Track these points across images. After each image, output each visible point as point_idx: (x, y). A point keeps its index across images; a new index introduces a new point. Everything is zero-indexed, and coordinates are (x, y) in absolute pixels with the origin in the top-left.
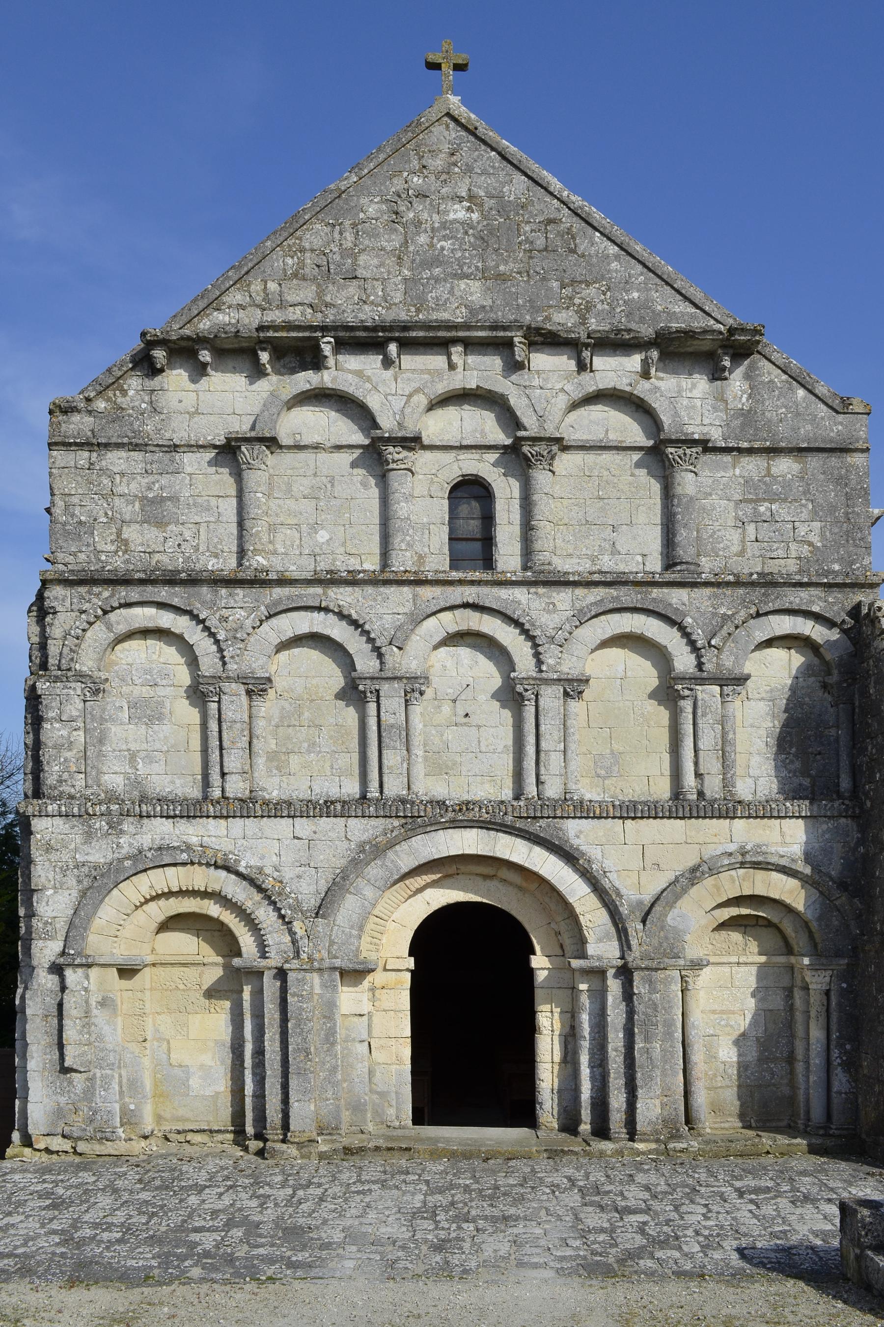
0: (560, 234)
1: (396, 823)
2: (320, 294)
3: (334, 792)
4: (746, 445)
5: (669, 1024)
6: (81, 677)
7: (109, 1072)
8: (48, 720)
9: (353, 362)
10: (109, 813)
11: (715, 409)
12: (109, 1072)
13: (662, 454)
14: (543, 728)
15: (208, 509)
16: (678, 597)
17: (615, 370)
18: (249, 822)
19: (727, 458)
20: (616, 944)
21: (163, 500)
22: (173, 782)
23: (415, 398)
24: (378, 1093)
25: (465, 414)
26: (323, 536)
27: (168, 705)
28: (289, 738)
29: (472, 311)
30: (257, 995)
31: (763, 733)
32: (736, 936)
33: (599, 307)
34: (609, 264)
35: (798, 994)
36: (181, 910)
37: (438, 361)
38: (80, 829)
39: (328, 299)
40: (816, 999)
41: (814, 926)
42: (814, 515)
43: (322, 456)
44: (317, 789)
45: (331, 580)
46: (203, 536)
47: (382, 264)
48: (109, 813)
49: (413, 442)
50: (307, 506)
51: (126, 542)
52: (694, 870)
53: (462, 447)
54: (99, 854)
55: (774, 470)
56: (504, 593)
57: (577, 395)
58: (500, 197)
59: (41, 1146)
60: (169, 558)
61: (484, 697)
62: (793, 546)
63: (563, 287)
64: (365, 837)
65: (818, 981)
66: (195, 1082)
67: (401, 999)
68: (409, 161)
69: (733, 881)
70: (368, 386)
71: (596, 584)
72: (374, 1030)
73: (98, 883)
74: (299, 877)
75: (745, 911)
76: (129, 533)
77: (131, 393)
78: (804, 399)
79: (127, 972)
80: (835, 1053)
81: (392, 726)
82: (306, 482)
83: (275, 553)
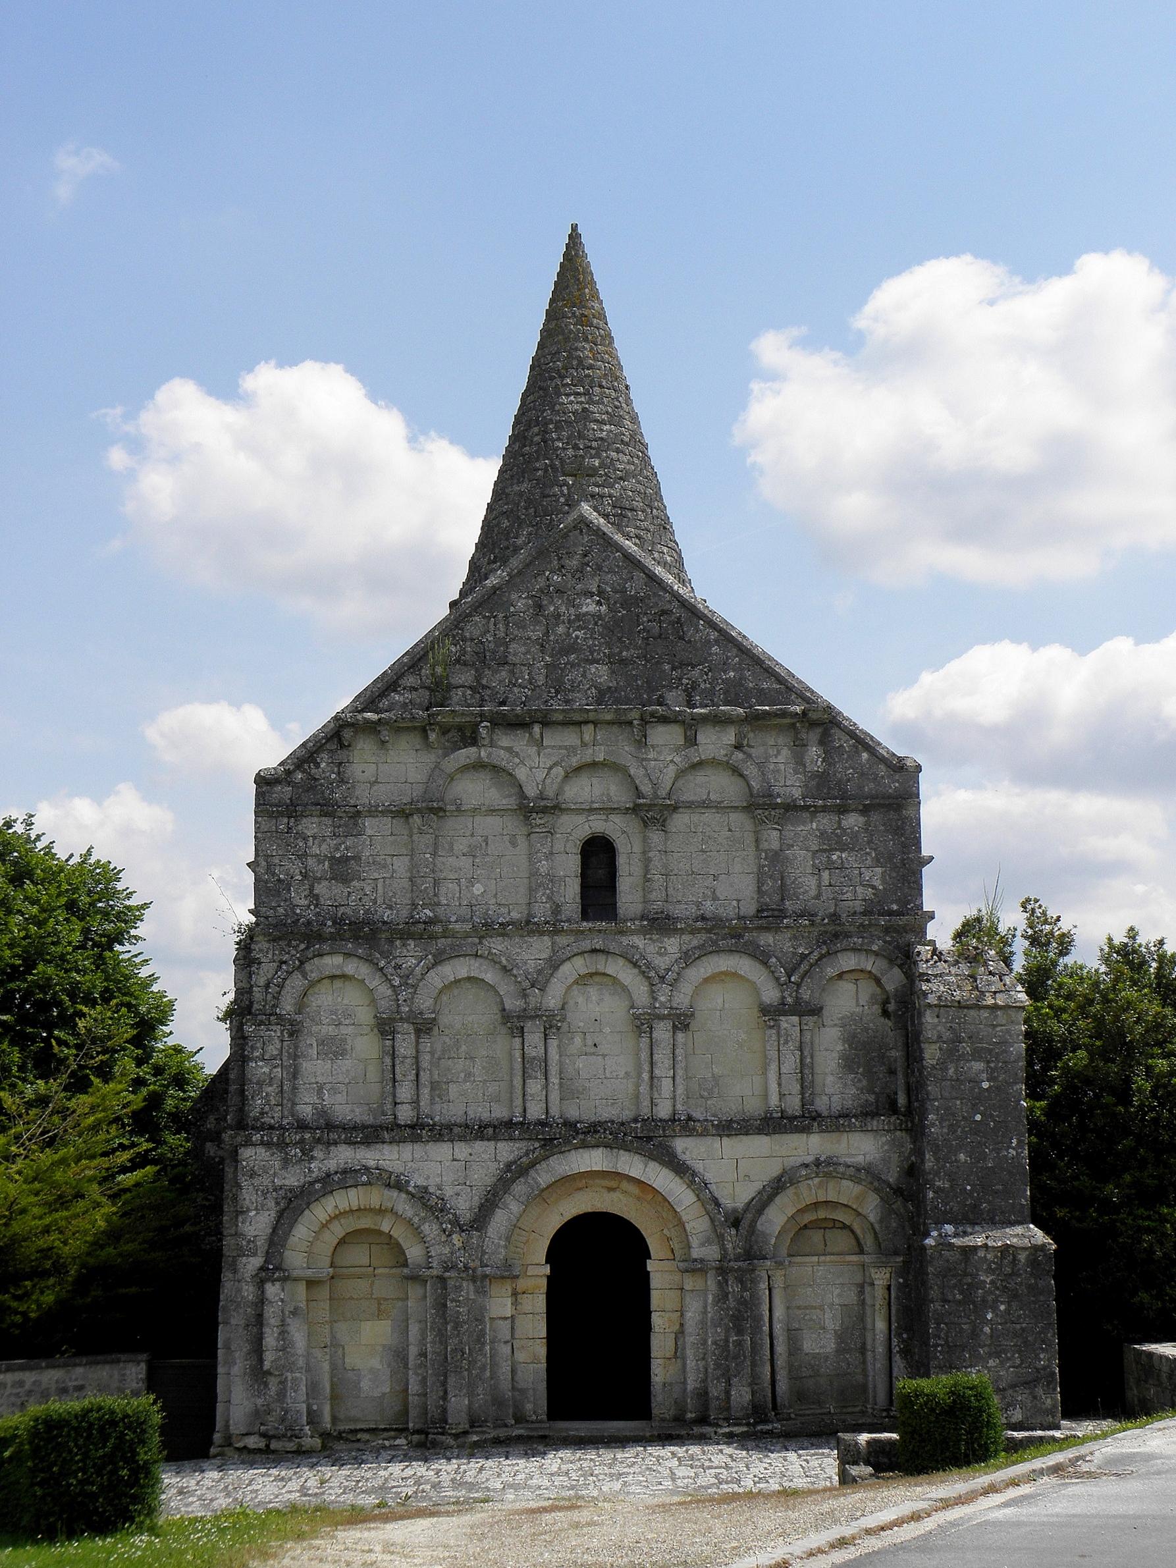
0: (672, 623)
1: (537, 1145)
2: (478, 679)
5: (758, 1319)
7: (298, 1375)
8: (251, 1059)
9: (505, 740)
10: (302, 1141)
12: (298, 1375)
13: (763, 806)
14: (656, 1057)
15: (385, 866)
18: (417, 1146)
21: (348, 859)
22: (353, 1111)
23: (554, 770)
24: (519, 1390)
25: (594, 780)
26: (478, 889)
27: (349, 1042)
31: (836, 1055)
33: (703, 686)
34: (710, 648)
35: (868, 1289)
36: (359, 1227)
37: (569, 737)
38: (279, 1156)
39: (484, 682)
40: (880, 1293)
41: (877, 1226)
44: (471, 1115)
46: (380, 890)
47: (528, 652)
48: (302, 1141)
50: (465, 862)
51: (317, 897)
52: (779, 1179)
54: (292, 1179)
55: (844, 823)
56: (625, 940)
58: (623, 591)
59: (240, 1445)
62: (859, 889)
63: (673, 669)
64: (511, 1158)
65: (881, 1277)
66: (365, 1385)
67: (537, 1303)
68: (551, 562)
69: (810, 1189)
70: (517, 760)
73: (292, 1205)
74: (458, 1194)
77: (323, 765)
78: (868, 760)
79: (311, 1283)
80: (895, 1341)
81: (534, 1058)
82: (465, 841)
83: (438, 904)
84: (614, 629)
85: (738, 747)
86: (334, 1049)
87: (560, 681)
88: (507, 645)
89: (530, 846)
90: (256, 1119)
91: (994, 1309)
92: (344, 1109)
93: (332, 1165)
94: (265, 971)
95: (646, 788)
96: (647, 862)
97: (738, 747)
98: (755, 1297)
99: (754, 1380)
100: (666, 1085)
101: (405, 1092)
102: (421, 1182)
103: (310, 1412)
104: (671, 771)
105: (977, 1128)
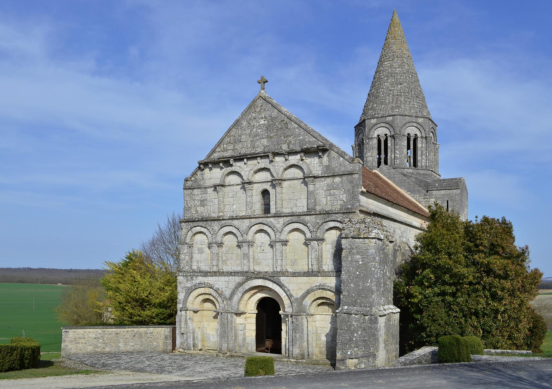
4: (326, 175)
9: (239, 164)
10: (191, 275)
11: (320, 166)
17: (294, 159)
19: (323, 179)
26: (235, 207)
29: (265, 147)
31: (330, 253)
32: (326, 307)
37: (255, 162)
42: (345, 193)
43: (235, 187)
45: (232, 219)
48: (191, 275)
49: (250, 183)
50: (231, 199)
54: (189, 285)
56: (269, 220)
57: (285, 167)
61: (267, 245)
66: (211, 338)
67: (252, 321)
71: (288, 216)
72: (247, 327)
73: (189, 291)
75: (324, 301)
76: (198, 209)
79: (195, 312)
82: (231, 194)
84: (268, 128)
85: (302, 160)
87: (254, 145)
88: (241, 136)
91: (357, 333)
92: (204, 268)
93: (197, 282)
99: (301, 347)
100: (279, 261)
104: (282, 169)
105: (358, 277)
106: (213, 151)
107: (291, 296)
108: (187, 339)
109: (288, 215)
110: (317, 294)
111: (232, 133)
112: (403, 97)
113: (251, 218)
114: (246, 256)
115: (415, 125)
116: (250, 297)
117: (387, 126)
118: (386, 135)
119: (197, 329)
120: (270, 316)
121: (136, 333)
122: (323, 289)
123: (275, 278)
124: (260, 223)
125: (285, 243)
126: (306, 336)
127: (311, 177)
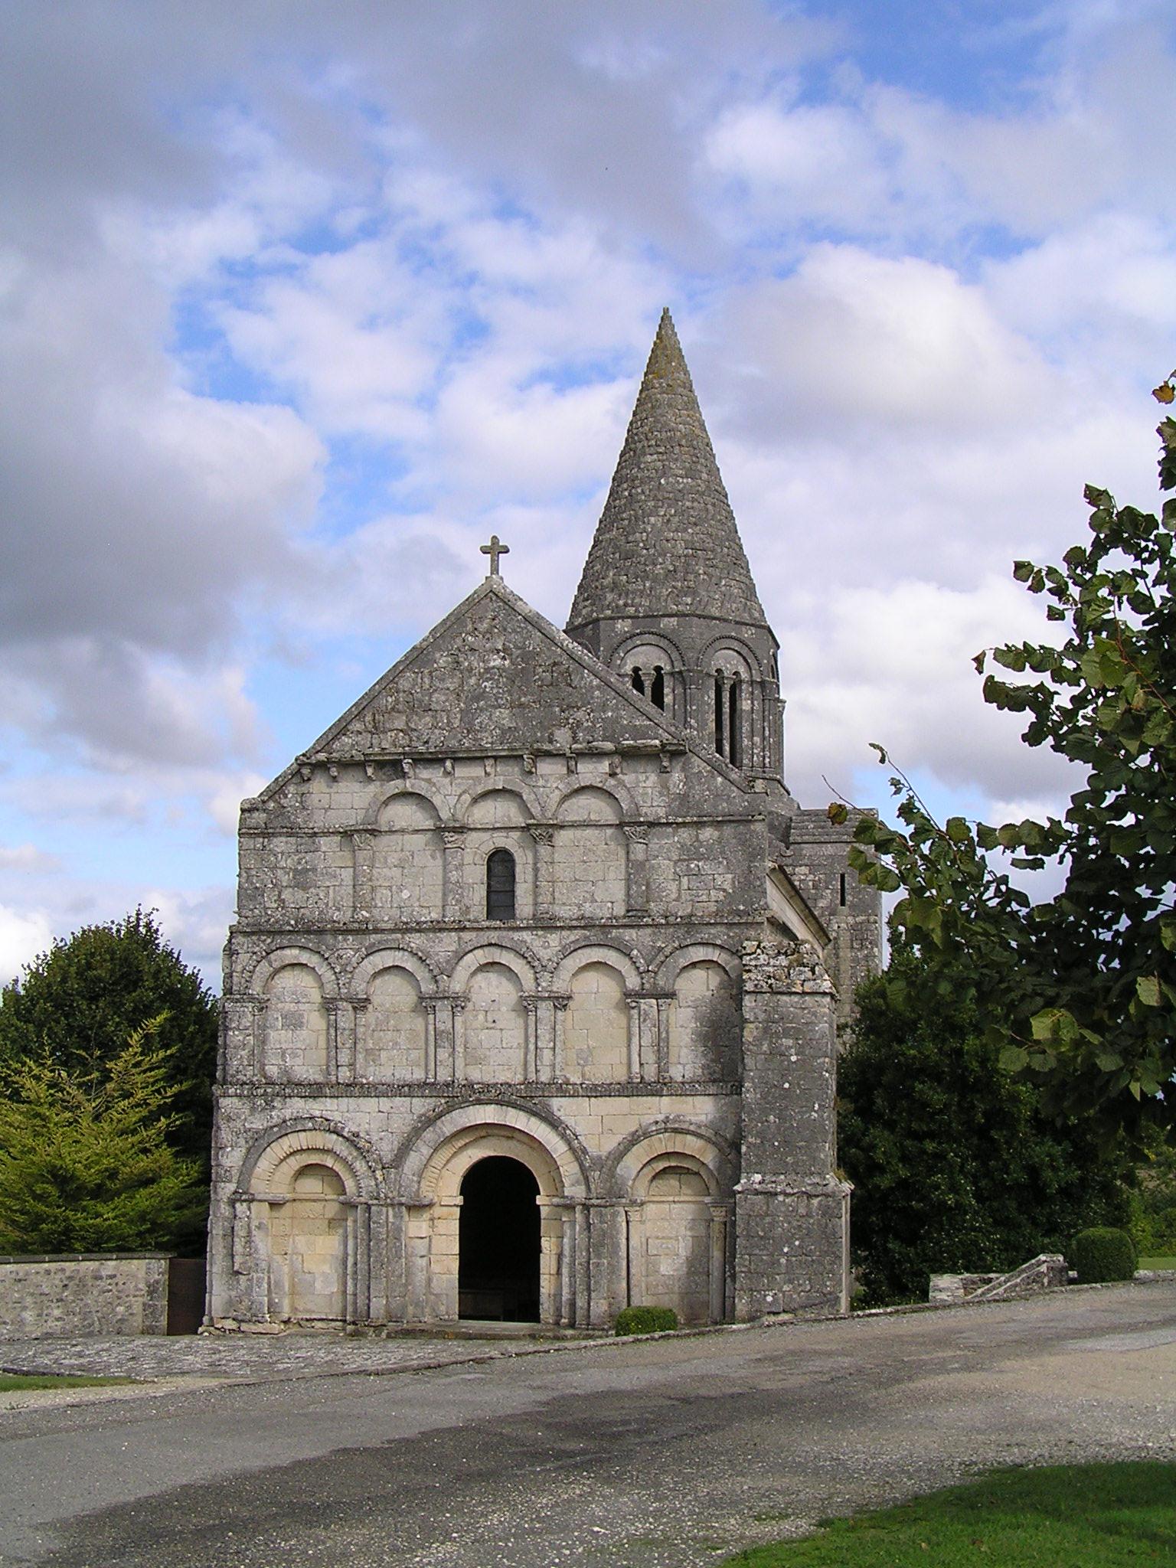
3: (409, 1078)
5: (616, 1246)
6: (252, 999)
9: (425, 773)
10: (265, 1094)
11: (661, 794)
13: (630, 826)
16: (630, 935)
17: (591, 772)
18: (351, 1100)
20: (583, 1187)
25: (498, 805)
26: (405, 894)
28: (380, 1039)
30: (367, 1223)
31: (689, 1031)
32: (673, 1182)
37: (476, 771)
42: (728, 869)
43: (407, 837)
45: (406, 929)
48: (265, 1094)
49: (462, 830)
53: (494, 829)
54: (258, 1123)
56: (516, 936)
59: (219, 1326)
60: (311, 913)
66: (318, 1285)
71: (575, 927)
72: (435, 1246)
73: (258, 1143)
75: (667, 1164)
79: (274, 1205)
82: (395, 855)
84: (518, 677)
85: (613, 775)
86: (294, 1022)
87: (471, 723)
89: (445, 860)
90: (233, 1076)
92: (307, 1071)
93: (287, 1114)
94: (243, 959)
95: (536, 810)
96: (536, 870)
97: (613, 775)
98: (614, 1225)
100: (547, 1055)
101: (344, 1057)
102: (354, 1129)
103: (270, 1304)
104: (556, 796)
106: (341, 729)
107: (585, 1151)
108: (249, 1290)
109: (575, 923)
110: (657, 1145)
111: (404, 684)
112: (701, 561)
113: (464, 929)
114: (443, 1038)
115: (736, 645)
116: (448, 1161)
117: (663, 643)
118: (658, 669)
119: (278, 1258)
120: (501, 1213)
121: (70, 1278)
122: (675, 1131)
123: (536, 1101)
124: (490, 945)
125: (561, 1002)
126: (624, 1263)
127: (641, 824)
